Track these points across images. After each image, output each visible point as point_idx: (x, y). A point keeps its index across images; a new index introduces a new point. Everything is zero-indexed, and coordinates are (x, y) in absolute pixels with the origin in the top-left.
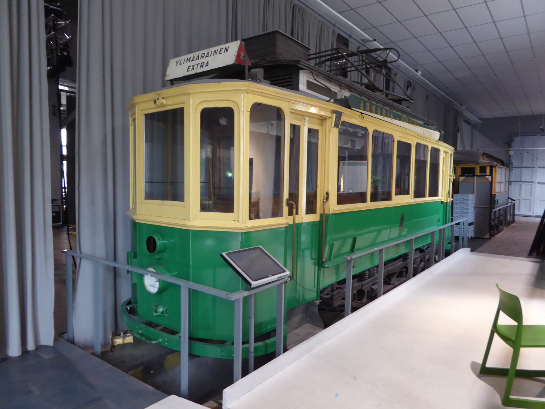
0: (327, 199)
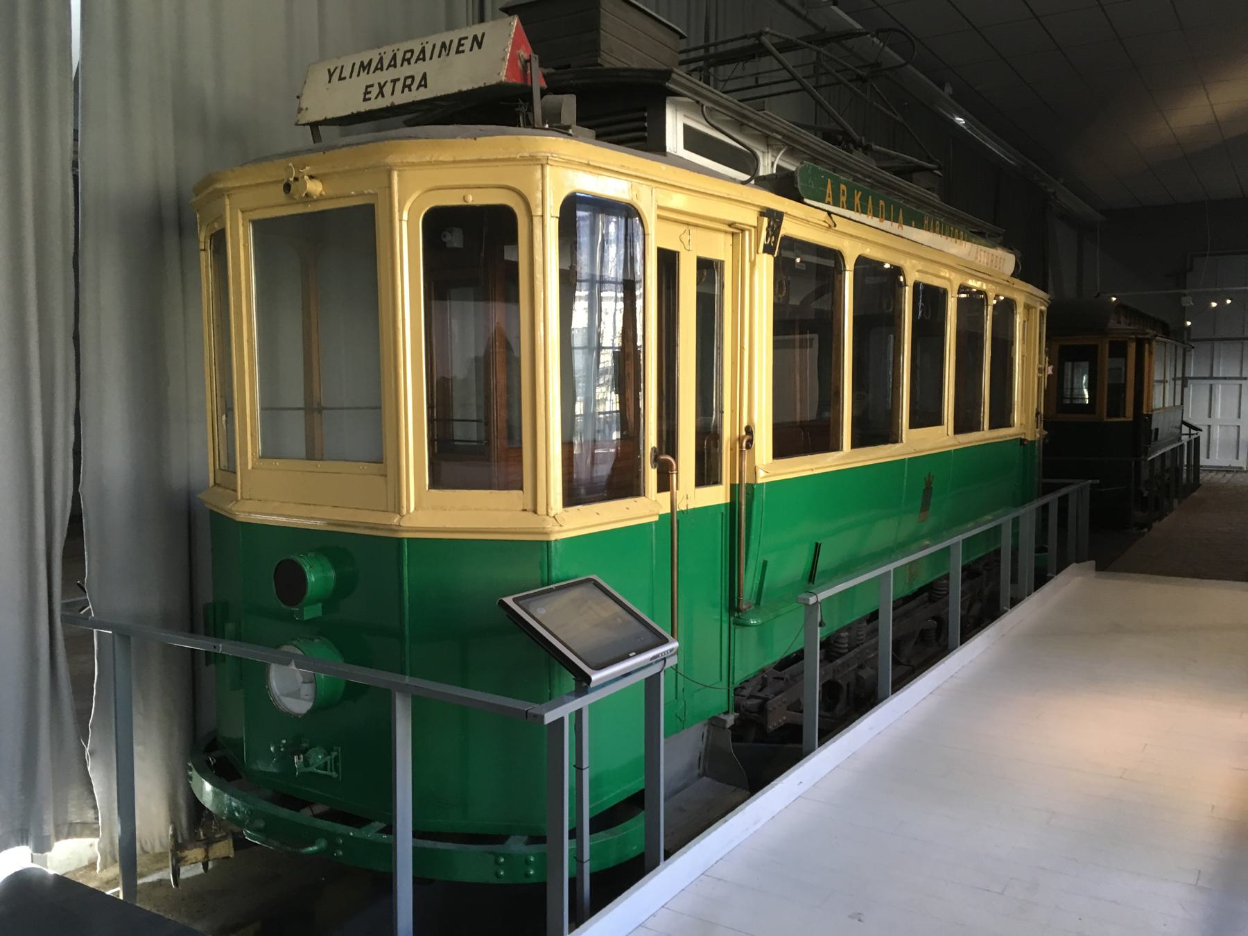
0: (750, 442)
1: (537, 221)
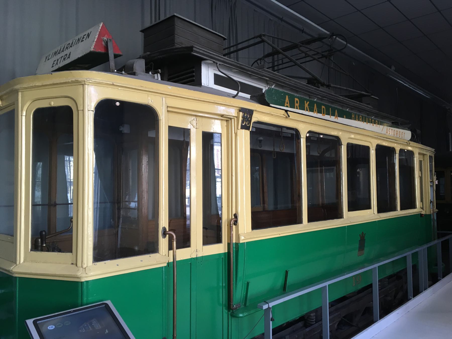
0: (236, 223)
1: (81, 113)
